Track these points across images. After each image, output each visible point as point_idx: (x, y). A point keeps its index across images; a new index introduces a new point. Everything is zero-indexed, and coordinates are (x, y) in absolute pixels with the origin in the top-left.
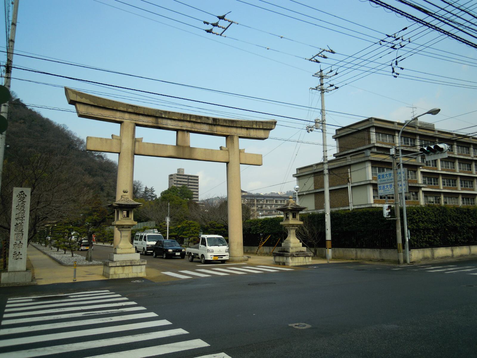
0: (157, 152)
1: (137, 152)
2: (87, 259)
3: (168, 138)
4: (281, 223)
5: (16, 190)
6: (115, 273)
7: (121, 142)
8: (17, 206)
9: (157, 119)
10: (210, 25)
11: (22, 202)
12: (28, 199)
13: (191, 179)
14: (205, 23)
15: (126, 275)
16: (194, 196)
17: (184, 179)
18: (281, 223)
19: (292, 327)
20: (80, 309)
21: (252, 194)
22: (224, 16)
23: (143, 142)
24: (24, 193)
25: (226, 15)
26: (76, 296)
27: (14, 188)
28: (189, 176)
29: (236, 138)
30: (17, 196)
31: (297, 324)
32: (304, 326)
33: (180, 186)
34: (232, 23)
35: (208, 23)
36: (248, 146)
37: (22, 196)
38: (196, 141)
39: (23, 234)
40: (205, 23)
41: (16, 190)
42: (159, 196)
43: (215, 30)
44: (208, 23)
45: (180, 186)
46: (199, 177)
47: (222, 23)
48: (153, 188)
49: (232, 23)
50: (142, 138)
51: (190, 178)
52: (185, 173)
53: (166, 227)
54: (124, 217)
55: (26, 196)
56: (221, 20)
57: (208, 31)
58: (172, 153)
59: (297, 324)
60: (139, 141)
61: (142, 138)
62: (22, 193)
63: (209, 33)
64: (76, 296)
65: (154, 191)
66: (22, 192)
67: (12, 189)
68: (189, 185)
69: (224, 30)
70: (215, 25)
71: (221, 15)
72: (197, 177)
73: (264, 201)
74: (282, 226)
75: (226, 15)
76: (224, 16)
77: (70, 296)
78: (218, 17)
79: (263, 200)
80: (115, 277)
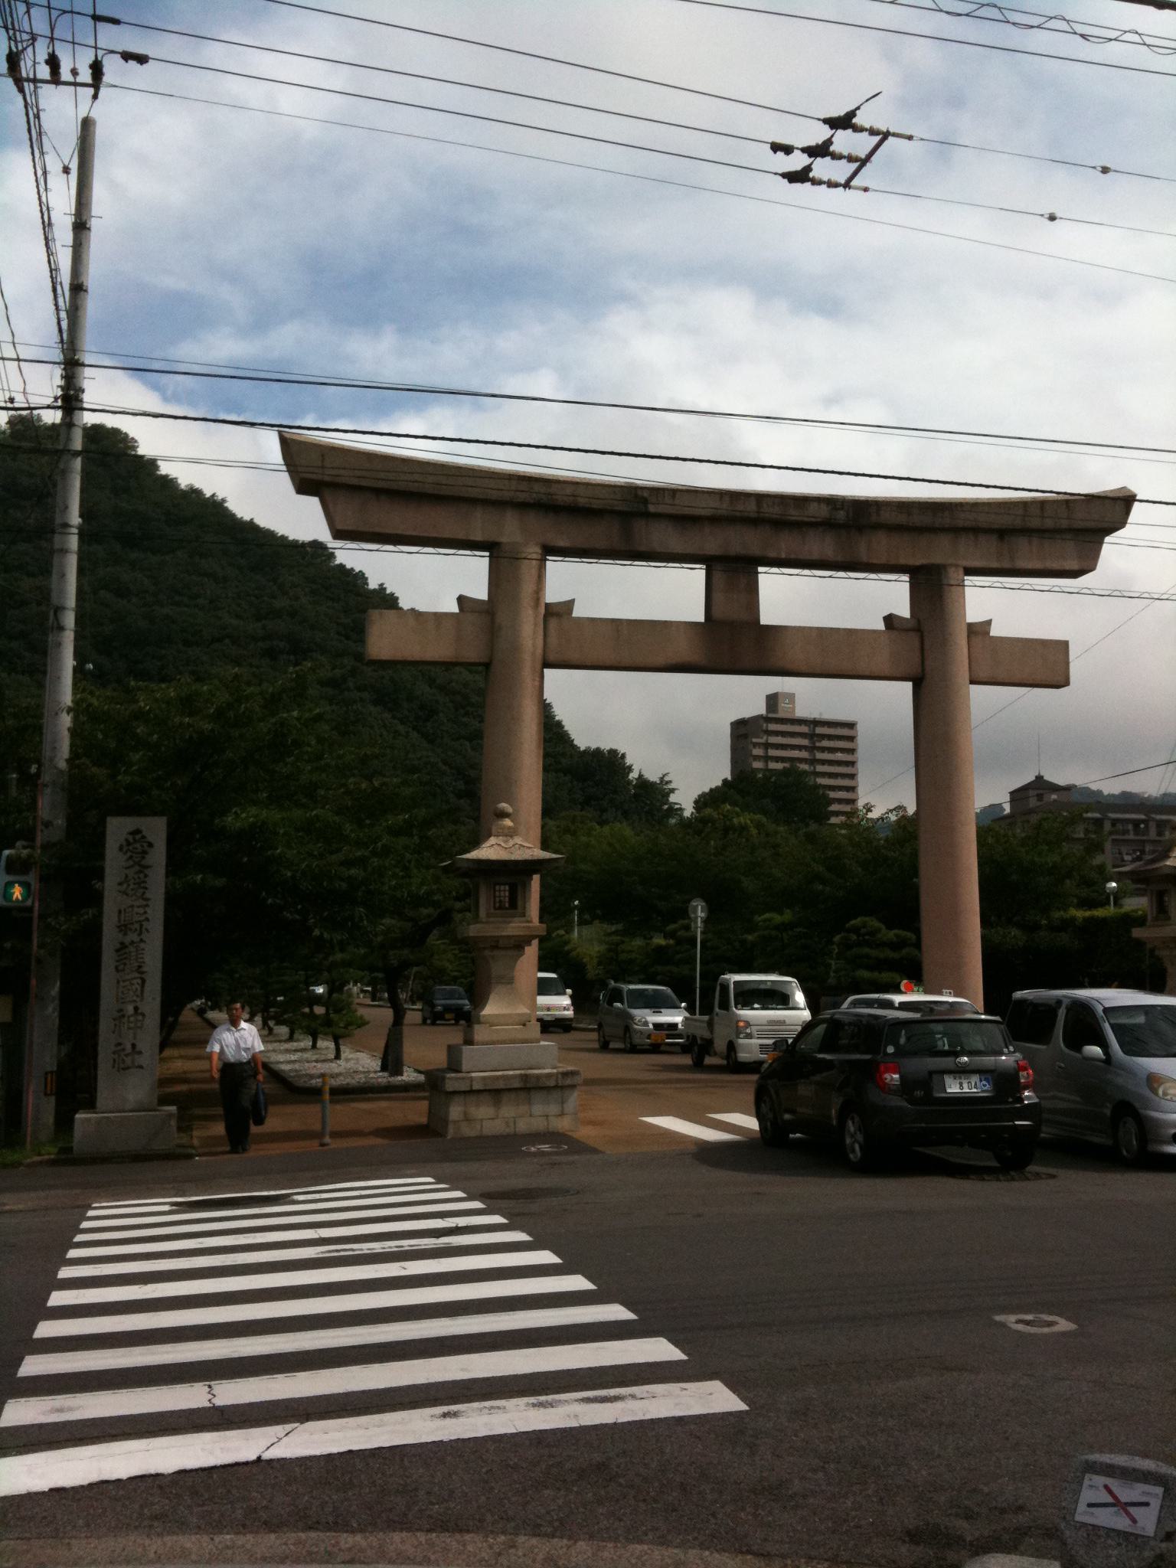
0: (633, 647)
1: (552, 657)
2: (384, 1068)
3: (676, 592)
4: (1137, 933)
5: (117, 828)
6: (467, 1119)
7: (493, 621)
8: (120, 884)
9: (626, 520)
10: (797, 153)
11: (137, 868)
12: (158, 857)
13: (830, 737)
14: (776, 147)
15: (507, 1124)
16: (834, 807)
17: (793, 735)
18: (1137, 933)
19: (1003, 1325)
20: (316, 1236)
21: (1100, 792)
22: (852, 114)
23: (575, 614)
24: (144, 837)
25: (858, 108)
26: (317, 1196)
27: (109, 819)
28: (816, 723)
29: (954, 575)
30: (121, 848)
31: (1030, 1317)
32: (1050, 1324)
33: (779, 766)
34: (886, 135)
35: (788, 150)
36: (998, 604)
37: (138, 845)
38: (786, 596)
39: (143, 981)
40: (776, 147)
41: (117, 828)
42: (688, 811)
43: (822, 168)
44: (788, 150)
45: (779, 766)
46: (859, 727)
47: (844, 141)
48: (667, 779)
49: (886, 135)
50: (573, 601)
51: (819, 730)
52: (800, 712)
53: (693, 941)
54: (500, 908)
55: (151, 845)
56: (840, 132)
57: (797, 177)
58: (683, 649)
59: (1030, 1317)
60: (558, 615)
61: (573, 601)
62: (138, 837)
63: (798, 185)
64: (317, 1196)
65: (673, 791)
66: (138, 831)
67: (103, 823)
68: (813, 762)
69: (855, 166)
70: (820, 151)
71: (840, 112)
72: (851, 725)
73: (1147, 827)
74: (1139, 944)
75: (858, 108)
76: (852, 114)
77: (296, 1197)
78: (826, 121)
79: (1143, 821)
80: (468, 1131)
